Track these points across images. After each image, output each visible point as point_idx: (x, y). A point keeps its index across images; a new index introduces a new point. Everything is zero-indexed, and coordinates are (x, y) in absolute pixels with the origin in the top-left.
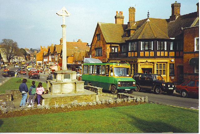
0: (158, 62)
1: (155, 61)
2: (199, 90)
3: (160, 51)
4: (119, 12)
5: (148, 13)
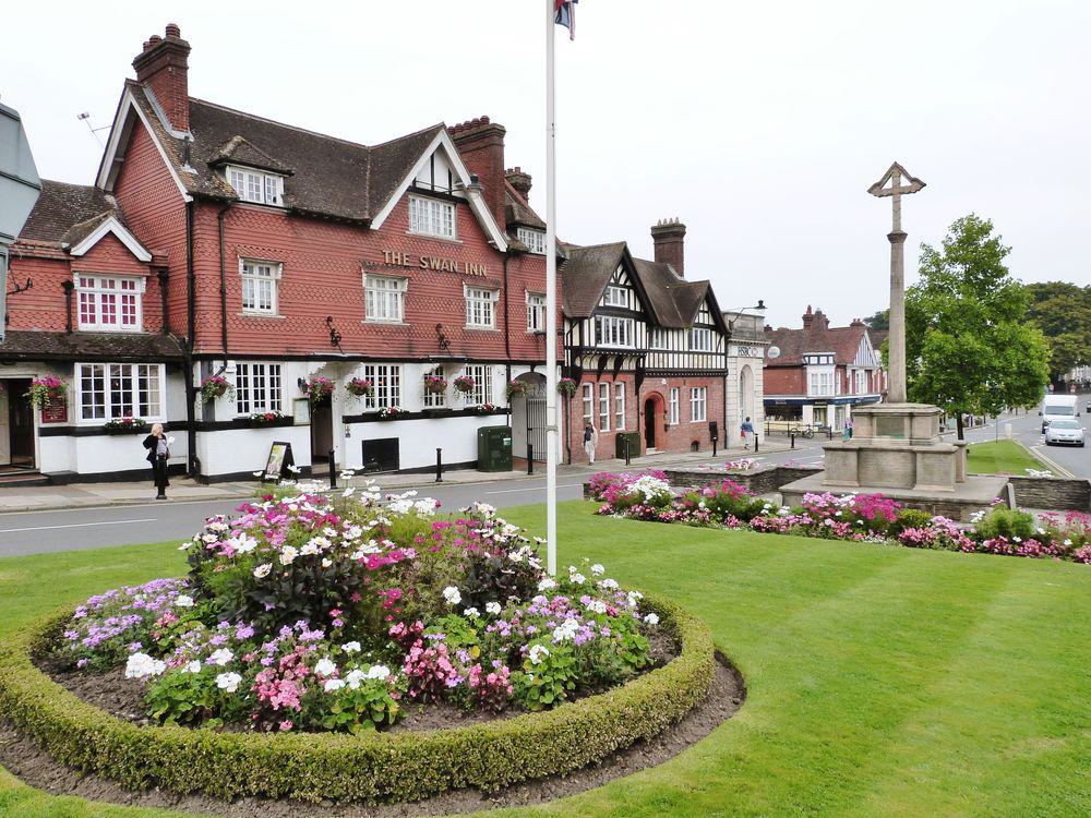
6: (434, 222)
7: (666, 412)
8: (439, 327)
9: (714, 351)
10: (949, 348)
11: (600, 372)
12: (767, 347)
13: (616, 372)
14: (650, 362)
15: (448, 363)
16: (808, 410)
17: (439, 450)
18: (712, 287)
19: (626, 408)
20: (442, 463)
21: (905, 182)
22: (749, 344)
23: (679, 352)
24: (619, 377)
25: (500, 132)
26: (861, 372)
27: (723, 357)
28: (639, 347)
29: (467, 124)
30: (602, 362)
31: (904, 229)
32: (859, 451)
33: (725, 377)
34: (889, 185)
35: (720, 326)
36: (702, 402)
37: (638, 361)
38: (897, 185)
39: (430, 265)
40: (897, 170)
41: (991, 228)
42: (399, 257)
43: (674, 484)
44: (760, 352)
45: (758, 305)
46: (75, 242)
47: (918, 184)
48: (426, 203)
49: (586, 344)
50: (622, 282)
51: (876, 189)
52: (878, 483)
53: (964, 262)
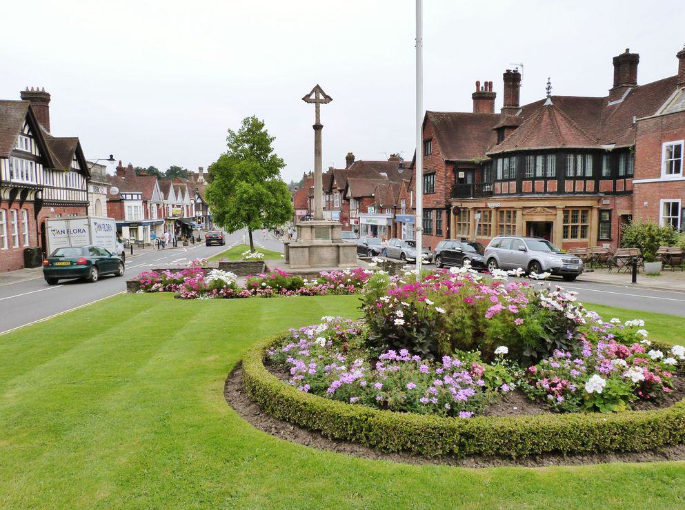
0: (566, 207)
1: (560, 204)
2: (454, 111)
3: (575, 178)
4: (482, 85)
5: (549, 83)
9: (80, 188)
10: (251, 191)
11: (11, 201)
12: (109, 187)
13: (22, 202)
14: (45, 195)
18: (80, 142)
19: (29, 229)
20: (627, 190)
21: (321, 97)
22: (99, 184)
24: (25, 205)
25: (615, 59)
26: (155, 206)
31: (322, 123)
32: (309, 247)
33: (87, 207)
34: (313, 97)
35: (84, 171)
38: (317, 97)
40: (318, 89)
41: (263, 125)
43: (238, 273)
44: (105, 190)
45: (109, 158)
47: (328, 99)
50: (26, 132)
51: (306, 99)
52: (320, 265)
53: (248, 142)
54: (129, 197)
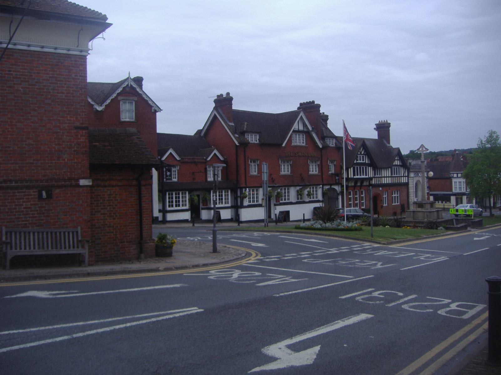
6: (299, 141)
7: (381, 200)
8: (301, 174)
9: (402, 175)
13: (361, 186)
15: (305, 186)
16: (453, 199)
17: (304, 214)
20: (305, 218)
23: (387, 177)
27: (407, 178)
28: (370, 176)
29: (307, 102)
30: (356, 183)
36: (398, 196)
37: (370, 181)
39: (298, 155)
42: (289, 154)
46: (207, 157)
48: (296, 134)
49: (350, 177)
50: (363, 153)
54: (455, 175)
